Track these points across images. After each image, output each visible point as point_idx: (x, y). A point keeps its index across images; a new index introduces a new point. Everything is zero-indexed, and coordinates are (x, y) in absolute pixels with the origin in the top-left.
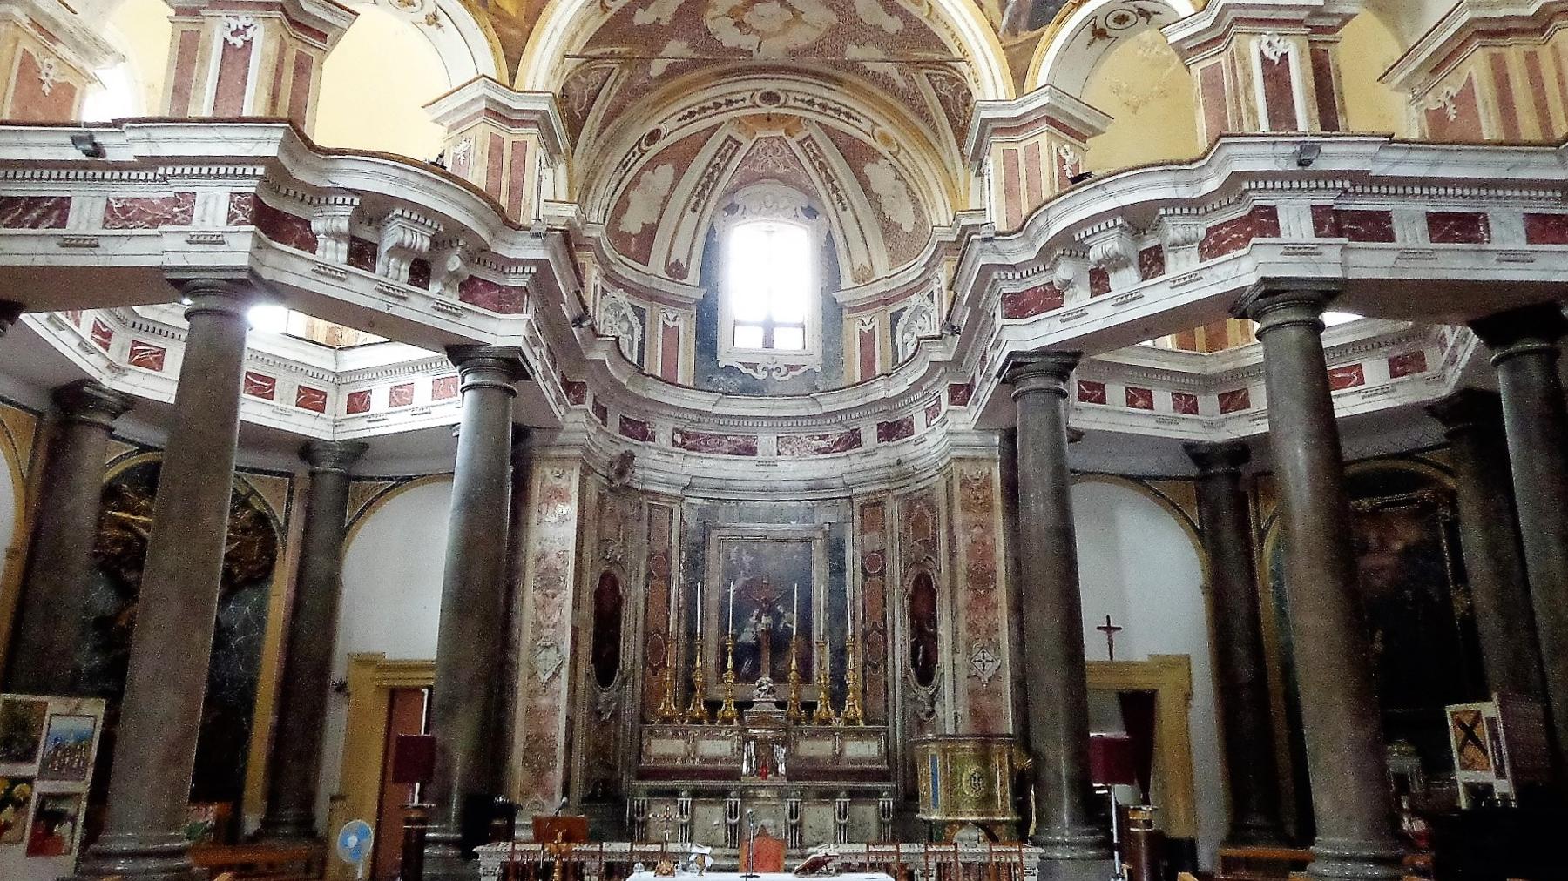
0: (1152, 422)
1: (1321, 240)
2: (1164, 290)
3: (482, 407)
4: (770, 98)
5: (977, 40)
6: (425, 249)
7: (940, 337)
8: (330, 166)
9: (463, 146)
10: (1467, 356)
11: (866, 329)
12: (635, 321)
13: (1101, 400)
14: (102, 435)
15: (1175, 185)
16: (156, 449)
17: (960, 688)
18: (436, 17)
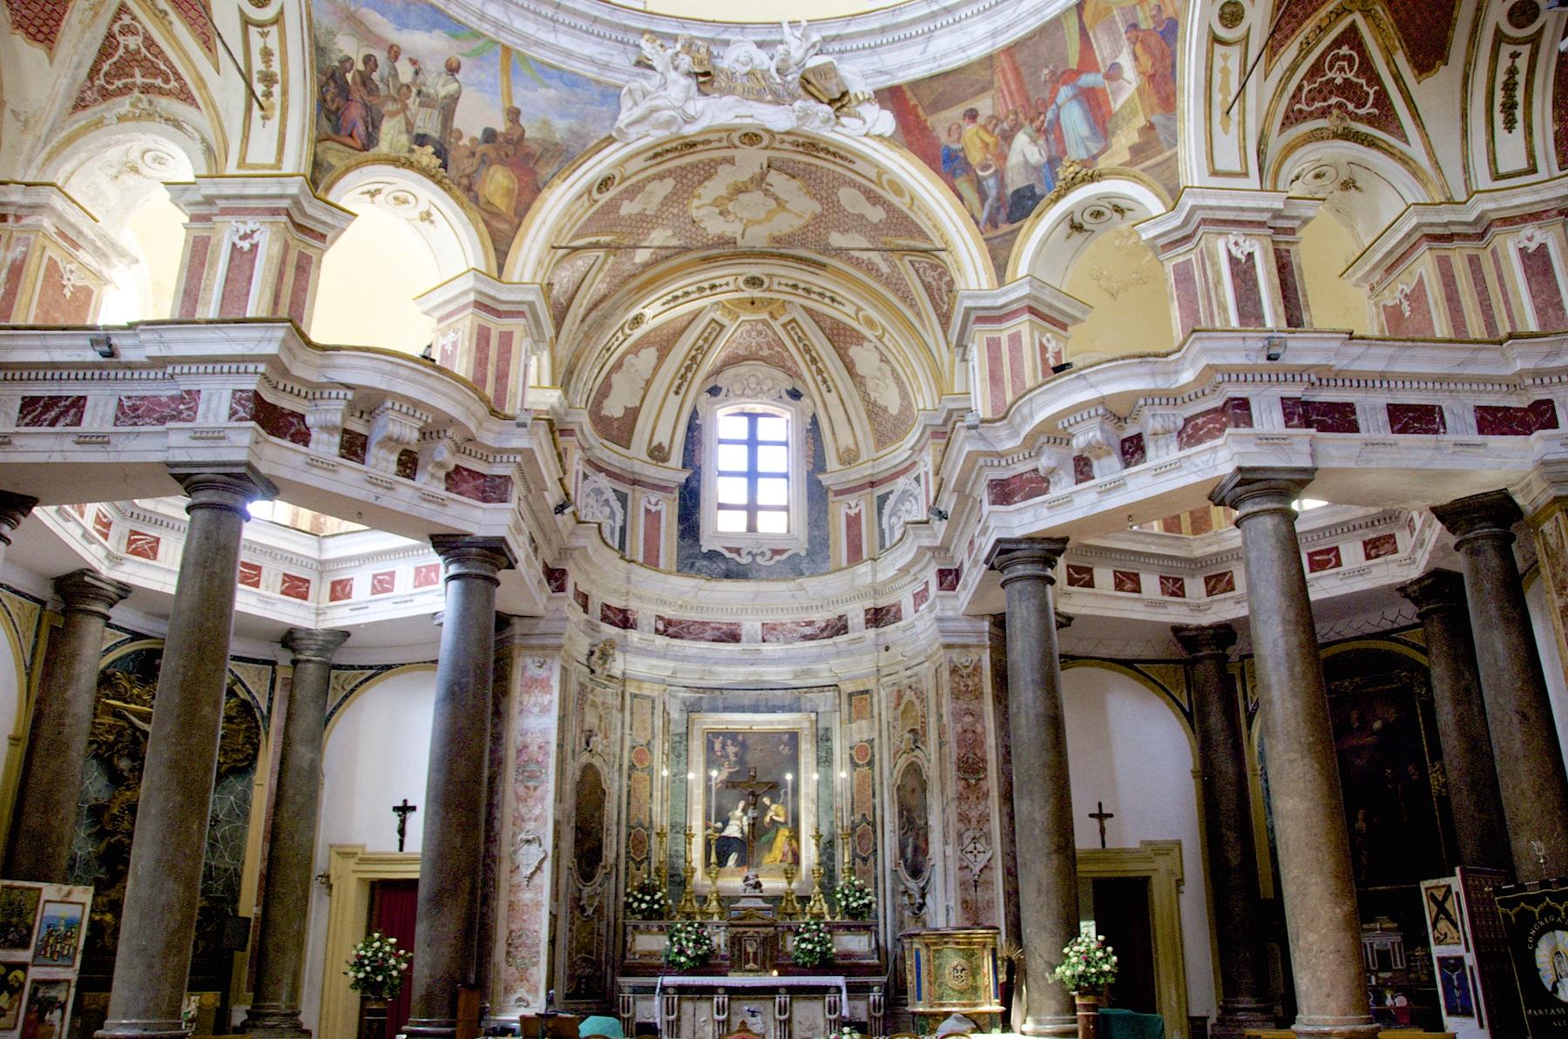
0: (1139, 606)
1: (1290, 431)
2: (1092, 496)
3: (467, 598)
4: (754, 282)
5: (958, 231)
6: (414, 441)
7: (927, 522)
8: (327, 362)
9: (451, 336)
10: (1434, 539)
11: (852, 512)
12: (617, 506)
13: (1090, 584)
14: (100, 623)
15: (1153, 375)
16: (149, 637)
17: (951, 879)
18: (429, 214)
